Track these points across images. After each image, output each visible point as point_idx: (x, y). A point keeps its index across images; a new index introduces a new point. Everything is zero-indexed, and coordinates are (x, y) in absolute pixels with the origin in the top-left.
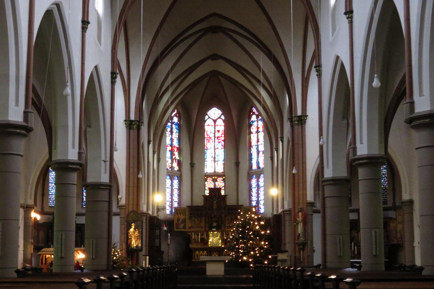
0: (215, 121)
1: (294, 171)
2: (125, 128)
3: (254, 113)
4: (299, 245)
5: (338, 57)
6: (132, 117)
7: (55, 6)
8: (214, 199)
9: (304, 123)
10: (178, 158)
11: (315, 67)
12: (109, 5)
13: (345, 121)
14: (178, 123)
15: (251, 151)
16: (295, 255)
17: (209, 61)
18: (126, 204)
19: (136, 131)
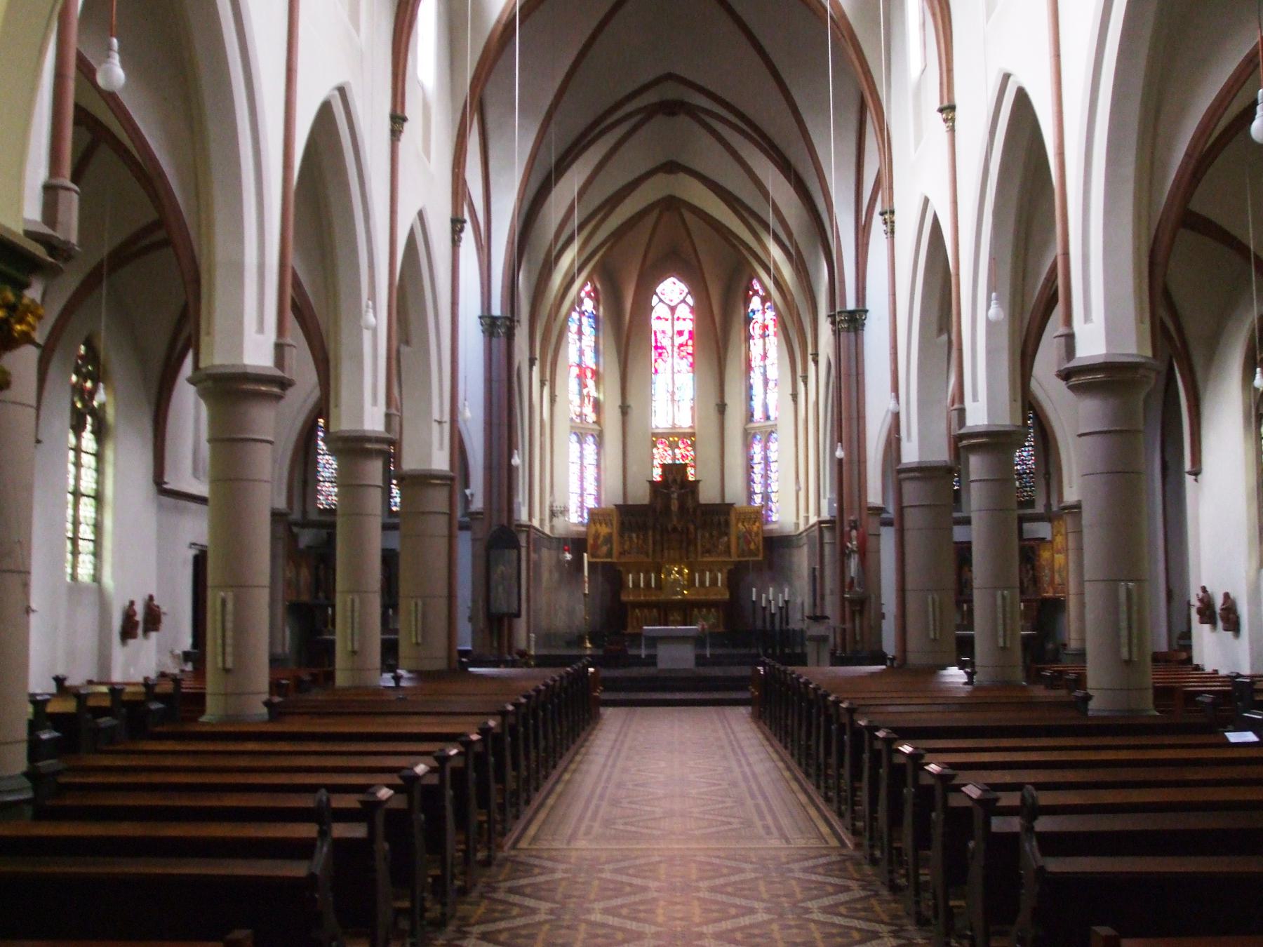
0: (673, 309)
1: (840, 453)
2: (482, 334)
3: (756, 293)
4: (851, 601)
5: (926, 201)
6: (496, 310)
7: (337, 93)
8: (673, 489)
9: (860, 328)
10: (594, 393)
11: (882, 214)
12: (446, 63)
13: (944, 337)
14: (594, 312)
15: (750, 377)
16: (844, 626)
17: (661, 178)
18: (483, 509)
19: (503, 340)
